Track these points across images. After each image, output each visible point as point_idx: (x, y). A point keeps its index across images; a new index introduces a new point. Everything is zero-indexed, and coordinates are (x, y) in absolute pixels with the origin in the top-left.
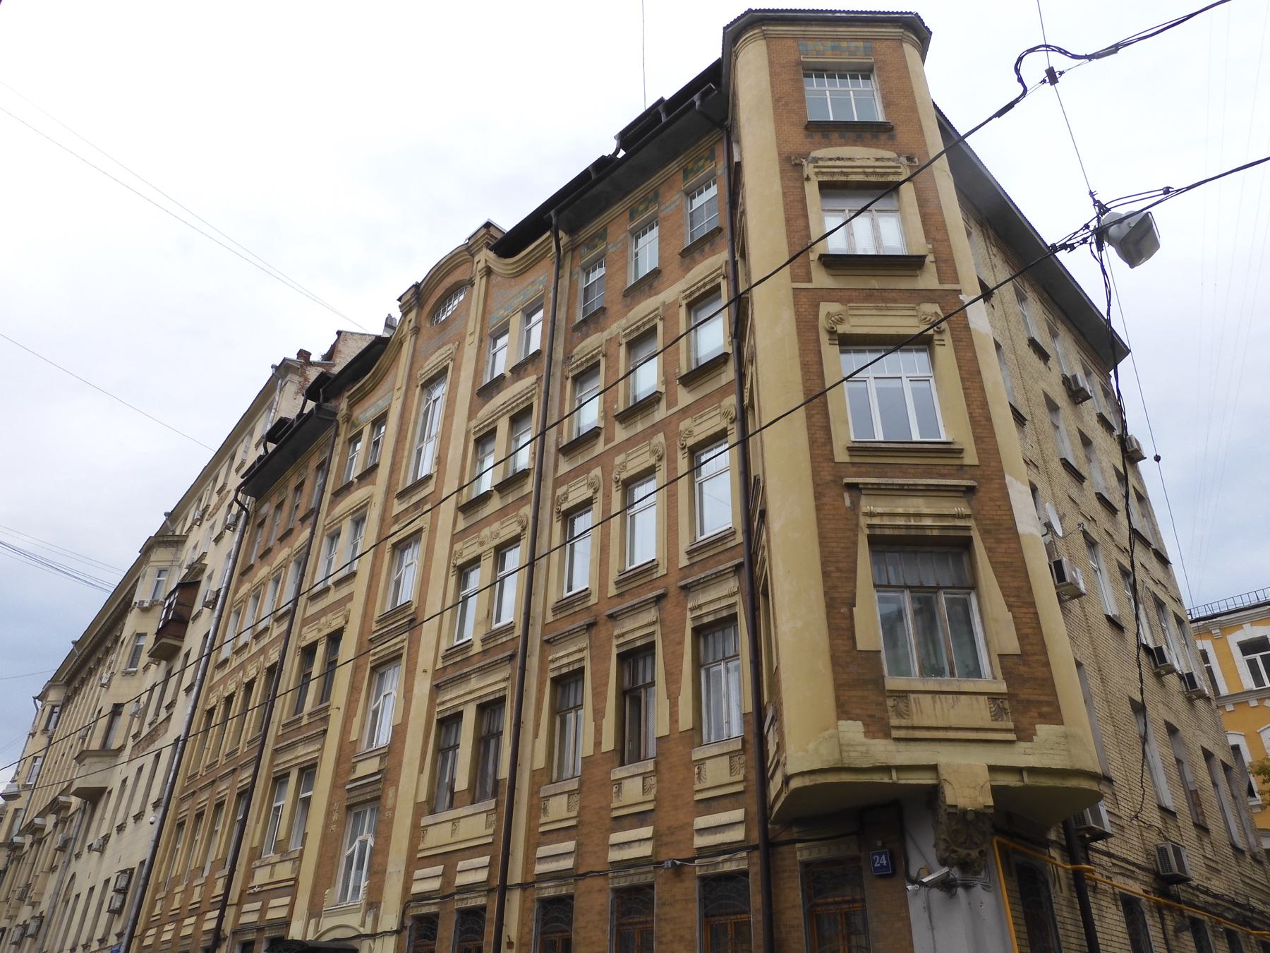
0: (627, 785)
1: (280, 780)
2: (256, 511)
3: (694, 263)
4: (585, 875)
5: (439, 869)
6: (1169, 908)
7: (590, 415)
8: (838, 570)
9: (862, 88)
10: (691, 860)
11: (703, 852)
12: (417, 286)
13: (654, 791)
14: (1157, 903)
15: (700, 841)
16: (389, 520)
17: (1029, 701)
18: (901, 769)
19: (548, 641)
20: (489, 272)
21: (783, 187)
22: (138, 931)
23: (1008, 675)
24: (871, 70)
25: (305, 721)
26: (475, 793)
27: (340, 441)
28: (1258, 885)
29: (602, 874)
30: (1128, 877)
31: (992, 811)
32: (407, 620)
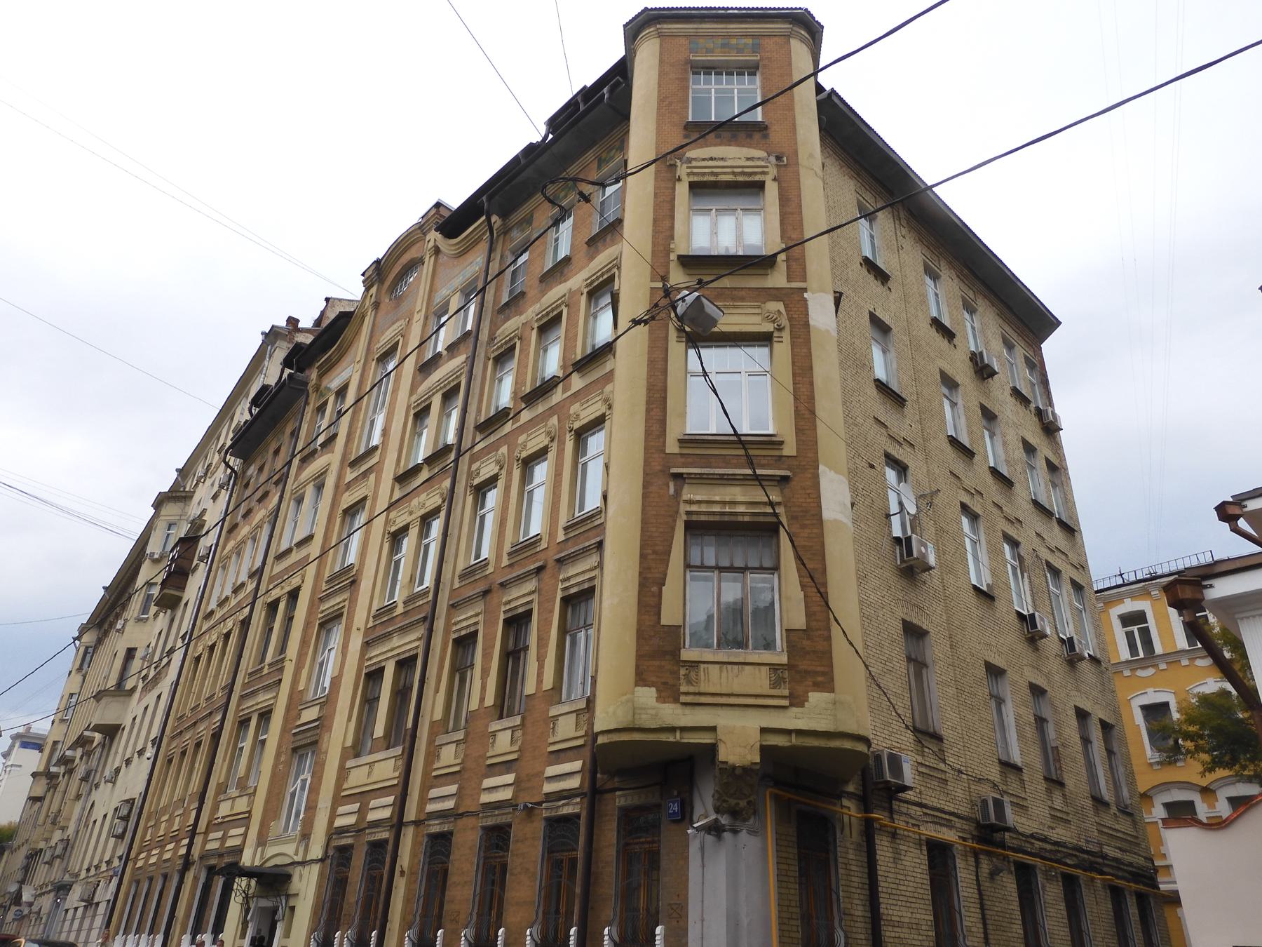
0: (500, 736)
1: (244, 723)
2: (244, 472)
3: (597, 252)
4: (462, 814)
5: (356, 806)
6: (989, 854)
7: (505, 397)
8: (655, 552)
9: (746, 86)
10: (540, 804)
11: (551, 797)
12: (378, 262)
13: (519, 743)
14: (973, 849)
15: (549, 788)
16: (342, 487)
17: (807, 672)
18: (684, 729)
19: (453, 606)
20: (437, 251)
21: (656, 188)
22: (132, 855)
23: (792, 648)
24: (757, 68)
25: (266, 671)
26: (389, 741)
27: (309, 409)
28: (1119, 835)
29: (474, 814)
30: (942, 825)
31: (758, 767)
32: (348, 580)
